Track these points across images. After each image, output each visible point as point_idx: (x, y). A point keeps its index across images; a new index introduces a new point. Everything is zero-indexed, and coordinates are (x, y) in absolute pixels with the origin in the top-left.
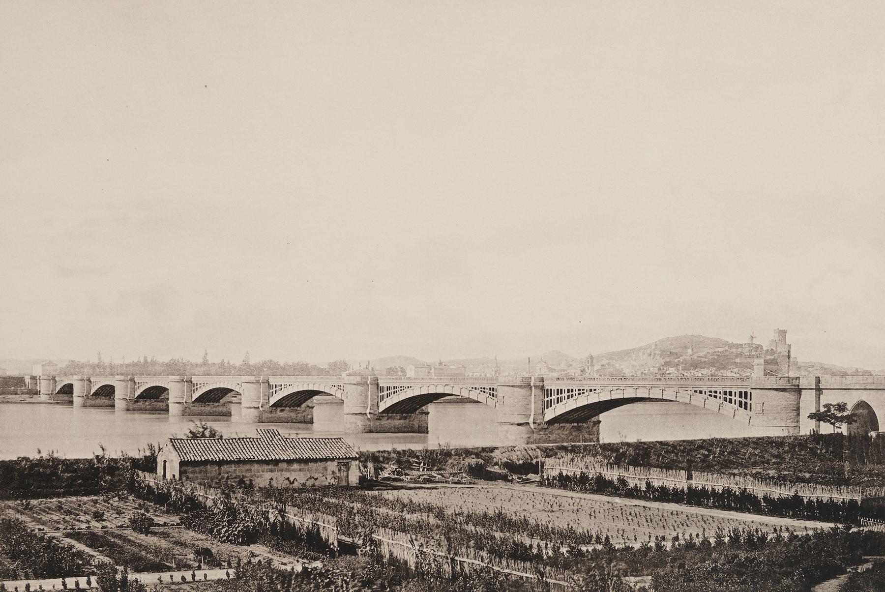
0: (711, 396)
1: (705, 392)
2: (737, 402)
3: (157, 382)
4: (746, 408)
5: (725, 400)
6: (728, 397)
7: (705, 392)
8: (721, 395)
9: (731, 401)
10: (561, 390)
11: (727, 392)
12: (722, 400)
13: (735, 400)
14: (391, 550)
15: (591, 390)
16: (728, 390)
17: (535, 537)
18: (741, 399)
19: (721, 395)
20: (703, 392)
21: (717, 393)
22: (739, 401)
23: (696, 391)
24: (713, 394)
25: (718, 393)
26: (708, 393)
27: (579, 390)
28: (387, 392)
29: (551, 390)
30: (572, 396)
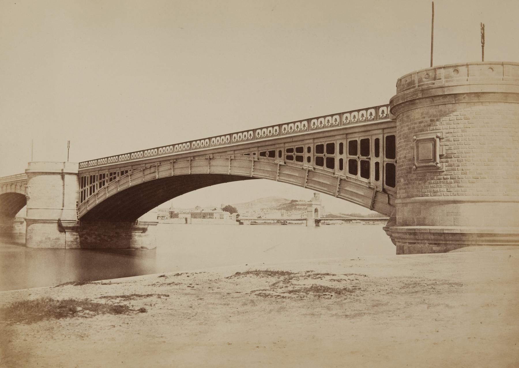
0: (290, 158)
1: (280, 152)
2: (346, 166)
3: (9, 187)
4: (366, 174)
5: (353, 170)
6: (325, 155)
7: (280, 152)
8: (311, 155)
9: (331, 164)
10: (104, 175)
11: (322, 145)
12: (313, 164)
13: (341, 161)
14: (232, 312)
15: (122, 173)
16: (325, 142)
17: (81, 314)
18: (353, 157)
19: (311, 155)
20: (277, 154)
21: (333, 144)
22: (350, 161)
23: (263, 154)
24: (295, 154)
25: (305, 150)
26: (284, 154)
27: (111, 174)
28: (91, 185)
29: (85, 177)
30: (115, 178)
